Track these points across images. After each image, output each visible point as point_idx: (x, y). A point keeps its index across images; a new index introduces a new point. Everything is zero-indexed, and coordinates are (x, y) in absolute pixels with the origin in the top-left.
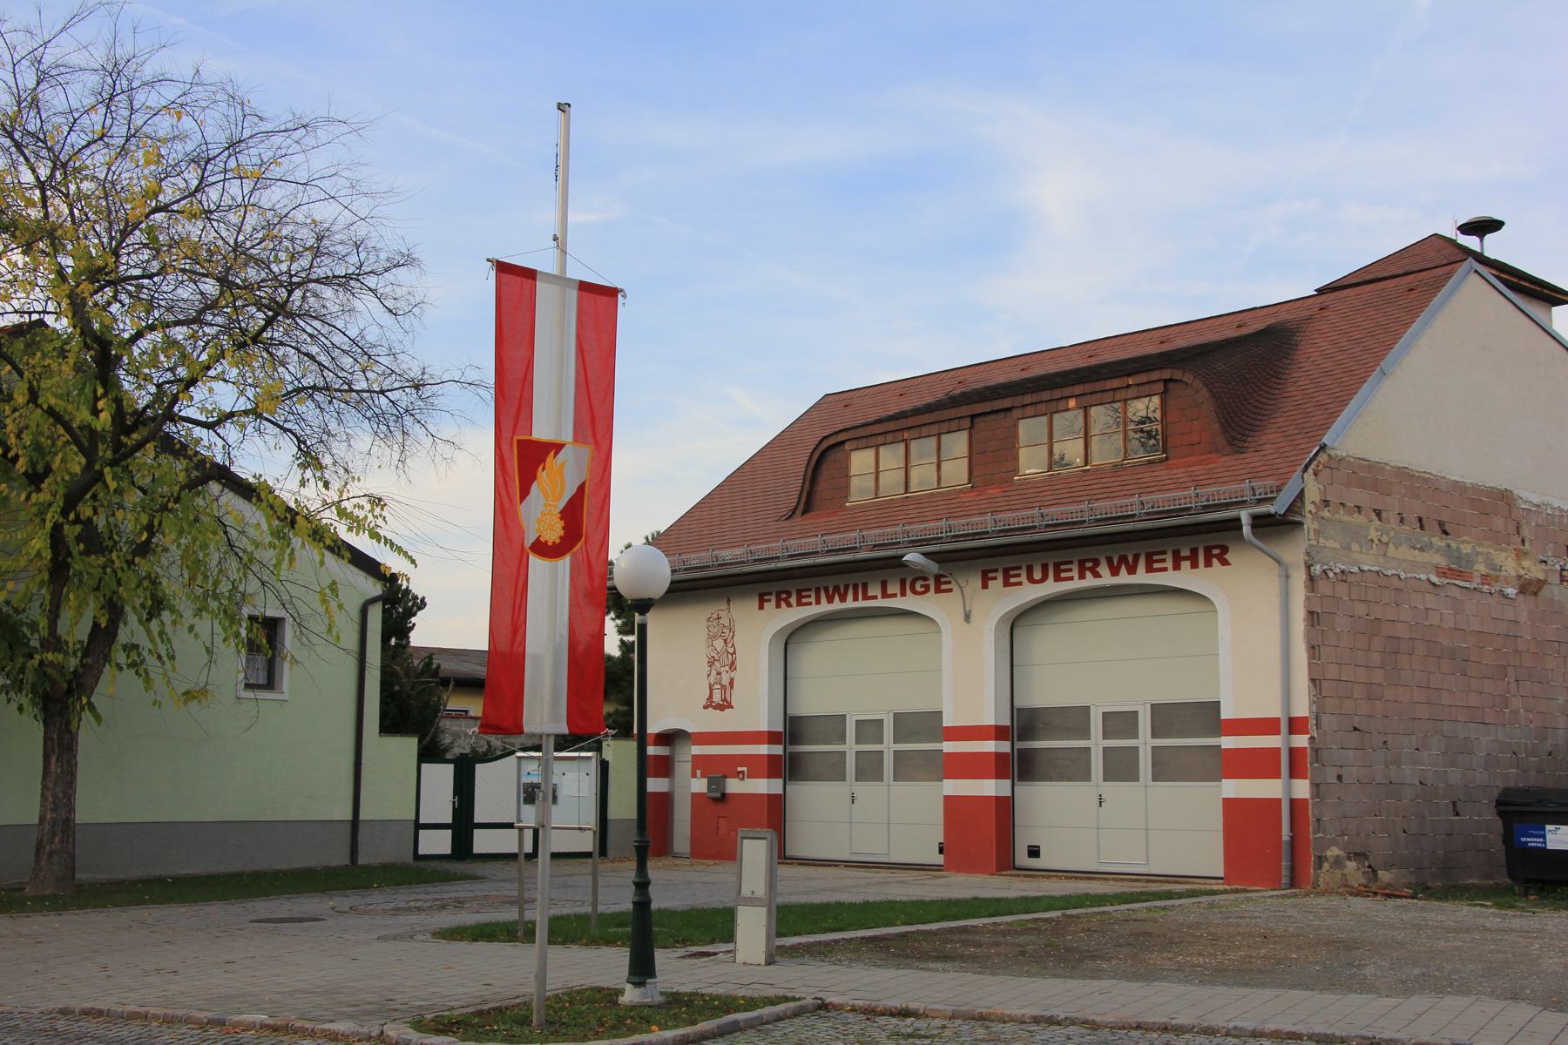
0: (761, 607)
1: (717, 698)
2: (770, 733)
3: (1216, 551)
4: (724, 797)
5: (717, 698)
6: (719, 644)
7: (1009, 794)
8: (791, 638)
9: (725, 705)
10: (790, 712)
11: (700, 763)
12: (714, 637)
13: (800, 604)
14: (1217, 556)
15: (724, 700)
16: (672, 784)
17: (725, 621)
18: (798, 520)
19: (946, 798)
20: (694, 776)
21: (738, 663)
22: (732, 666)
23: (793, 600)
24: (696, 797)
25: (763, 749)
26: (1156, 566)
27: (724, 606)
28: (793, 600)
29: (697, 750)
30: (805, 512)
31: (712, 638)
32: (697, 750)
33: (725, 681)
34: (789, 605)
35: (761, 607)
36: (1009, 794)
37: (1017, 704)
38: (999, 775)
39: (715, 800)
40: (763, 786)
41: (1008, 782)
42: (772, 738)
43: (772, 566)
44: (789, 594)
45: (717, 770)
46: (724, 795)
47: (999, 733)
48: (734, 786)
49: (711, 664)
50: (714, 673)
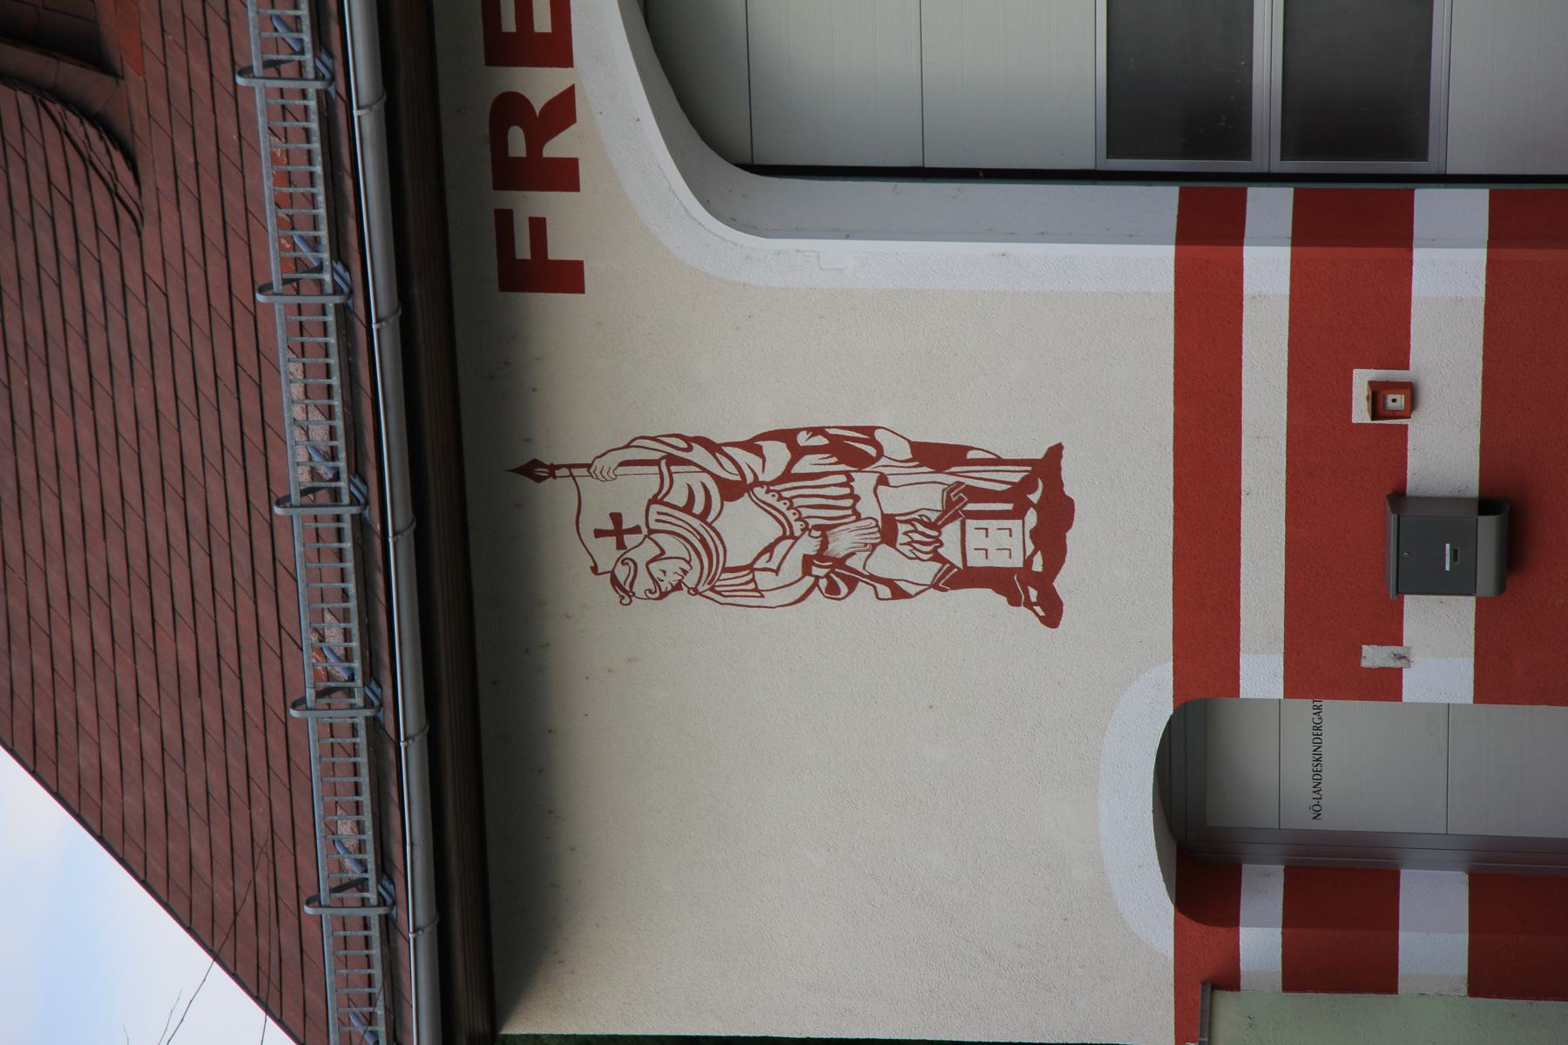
0: (569, 277)
1: (1003, 543)
2: (1186, 236)
3: (517, 143)
4: (1501, 498)
5: (1003, 543)
6: (745, 528)
7: (1478, 200)
8: (738, 141)
9: (1043, 494)
10: (1086, 151)
11: (1337, 651)
12: (709, 548)
13: (557, 50)
14: (535, 144)
15: (1017, 496)
16: (1436, 850)
17: (631, 494)
18: (138, 96)
19: (1478, 698)
20: (1387, 685)
21: (841, 415)
22: (852, 449)
23: (540, 85)
24: (1494, 681)
25: (1267, 268)
26: (543, 22)
27: (559, 491)
28: (540, 85)
29: (1261, 671)
30: (93, 55)
31: (719, 578)
32: (1261, 671)
33: (920, 494)
34: (563, 110)
35: (569, 277)
36: (1478, 200)
37: (1087, 156)
38: (1396, 233)
39: (1512, 556)
40: (1449, 271)
41: (1426, 200)
42: (1209, 230)
43: (366, 122)
44: (511, 108)
45: (1365, 545)
46: (1486, 505)
47: (1209, 230)
48: (1445, 447)
49: (836, 576)
50: (886, 562)
